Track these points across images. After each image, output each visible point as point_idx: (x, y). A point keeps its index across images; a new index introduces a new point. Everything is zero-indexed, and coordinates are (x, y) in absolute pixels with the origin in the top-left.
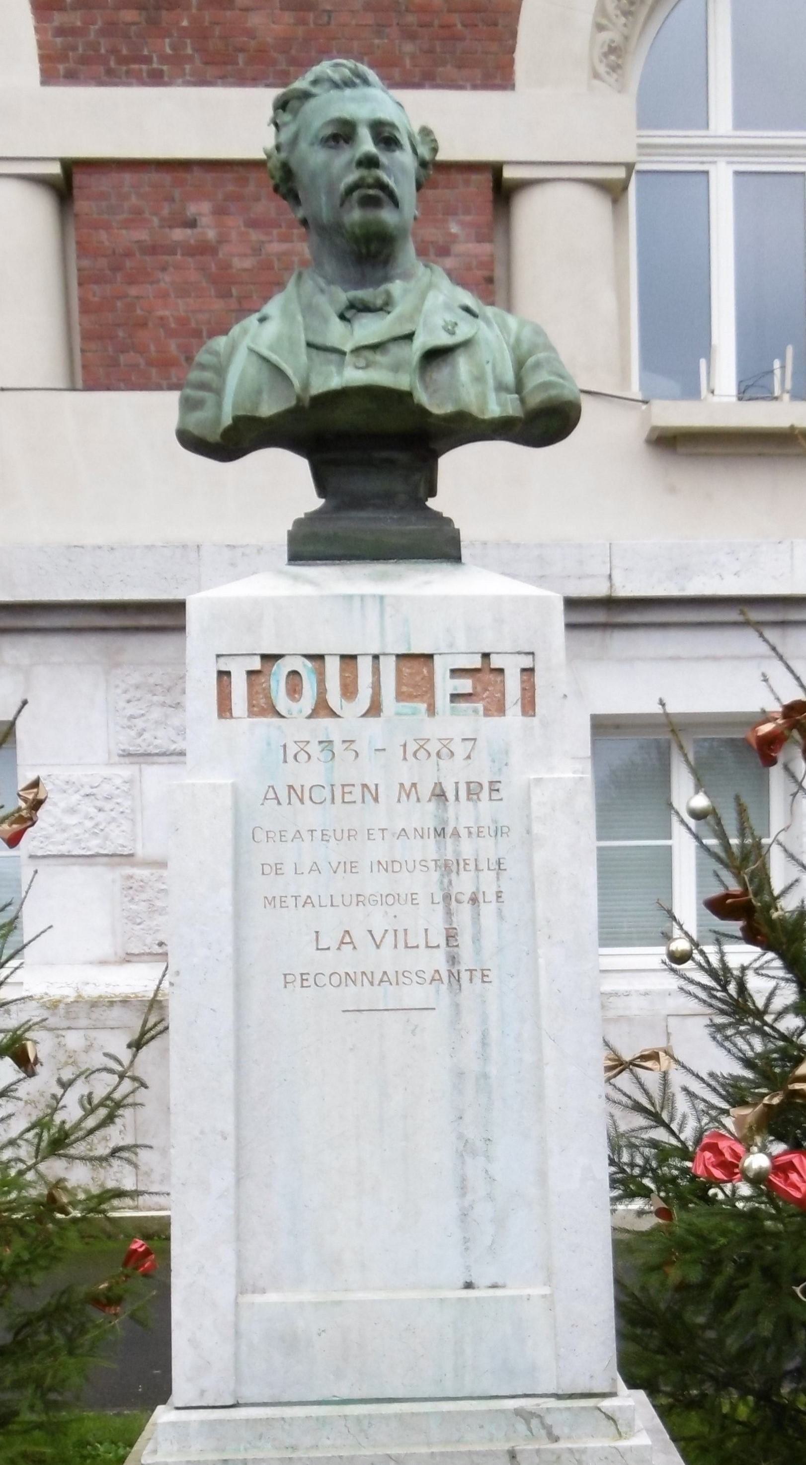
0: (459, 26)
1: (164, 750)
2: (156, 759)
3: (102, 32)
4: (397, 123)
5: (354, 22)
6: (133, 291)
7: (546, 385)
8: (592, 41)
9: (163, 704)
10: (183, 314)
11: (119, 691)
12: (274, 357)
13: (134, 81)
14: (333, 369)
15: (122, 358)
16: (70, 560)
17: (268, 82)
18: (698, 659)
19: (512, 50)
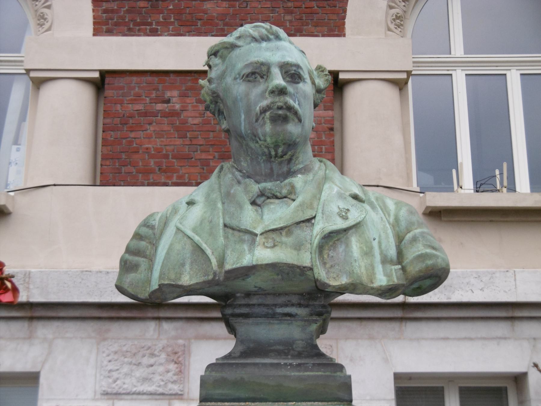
0: (316, 8)
1: (128, 391)
2: (123, 396)
3: (128, 11)
4: (301, 65)
5: (260, 6)
6: (132, 135)
7: (422, 257)
8: (387, 14)
9: (130, 363)
10: (159, 146)
11: (105, 355)
12: (197, 238)
13: (142, 33)
14: (246, 247)
15: (123, 169)
16: (83, 279)
17: (213, 34)
18: (459, 339)
19: (344, 18)
